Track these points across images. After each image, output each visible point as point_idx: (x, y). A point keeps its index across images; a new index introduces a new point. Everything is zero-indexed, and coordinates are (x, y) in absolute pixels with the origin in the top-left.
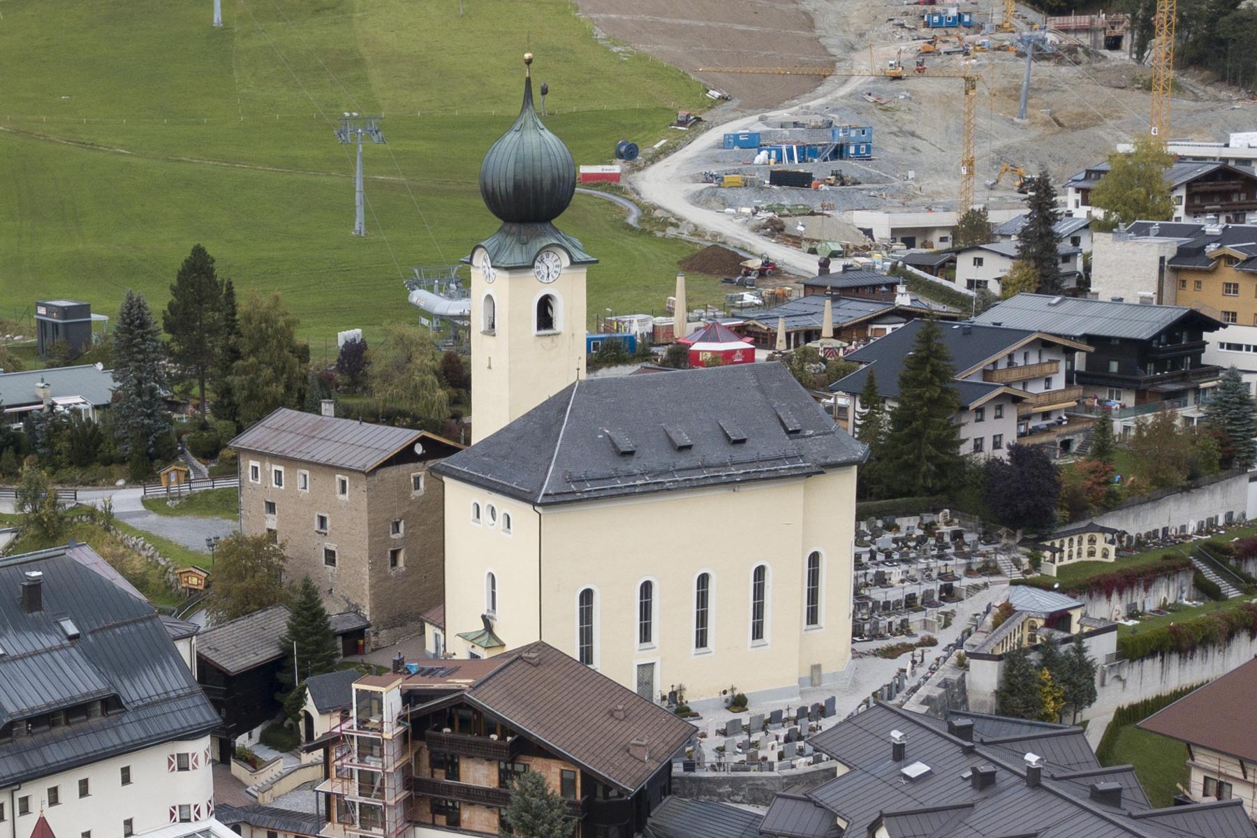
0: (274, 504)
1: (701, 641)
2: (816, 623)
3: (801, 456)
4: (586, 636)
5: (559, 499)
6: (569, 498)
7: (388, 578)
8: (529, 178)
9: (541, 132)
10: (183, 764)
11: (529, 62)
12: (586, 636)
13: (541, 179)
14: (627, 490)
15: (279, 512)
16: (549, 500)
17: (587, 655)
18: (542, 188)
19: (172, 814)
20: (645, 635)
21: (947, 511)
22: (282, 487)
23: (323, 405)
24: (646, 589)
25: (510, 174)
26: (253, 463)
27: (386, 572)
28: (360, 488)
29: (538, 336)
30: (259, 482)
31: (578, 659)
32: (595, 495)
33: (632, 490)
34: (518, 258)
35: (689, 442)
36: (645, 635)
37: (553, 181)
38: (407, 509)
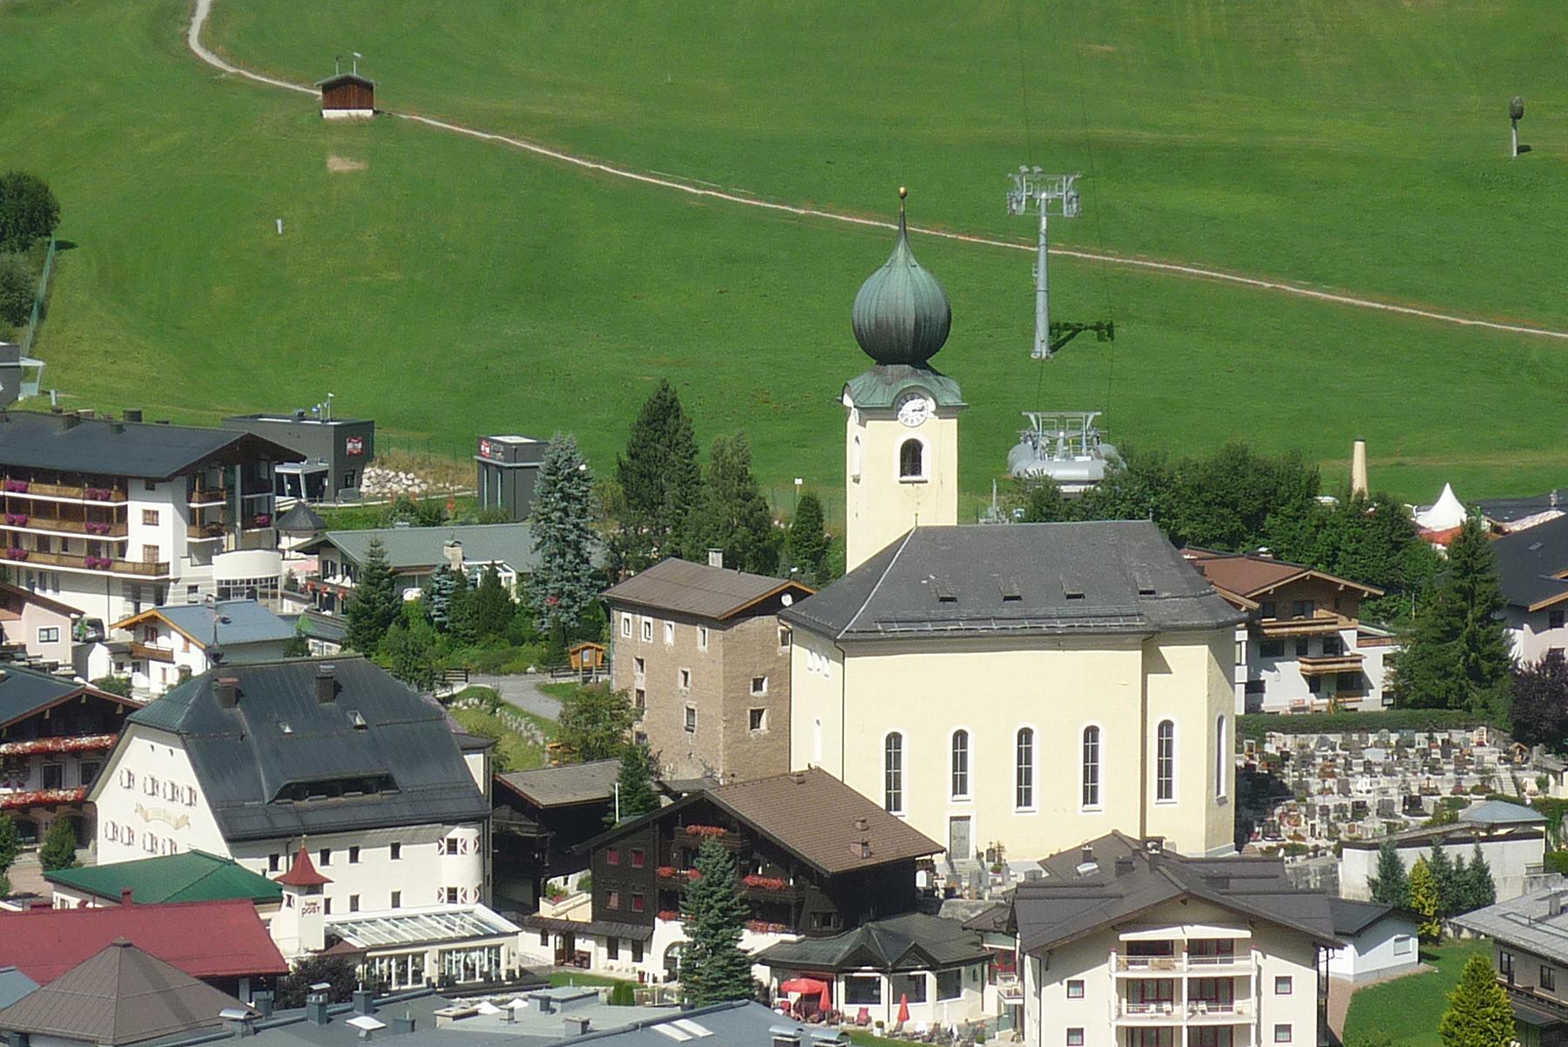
0: (1276, 1026)
1: (1024, 798)
2: (1170, 797)
3: (1139, 615)
4: (893, 782)
5: (860, 636)
6: (872, 636)
7: (746, 740)
8: (892, 318)
9: (912, 269)
10: (452, 847)
11: (903, 196)
12: (893, 782)
13: (904, 319)
14: (936, 634)
15: (648, 670)
16: (851, 636)
17: (894, 801)
18: (905, 328)
19: (440, 895)
20: (960, 785)
21: (1484, 728)
22: (651, 642)
23: (710, 554)
24: (960, 738)
25: (910, 304)
26: (625, 615)
27: (744, 732)
28: (717, 638)
29: (902, 482)
30: (630, 637)
31: (884, 808)
32: (900, 635)
33: (941, 633)
34: (881, 398)
35: (1017, 593)
36: (960, 785)
37: (917, 323)
38: (771, 666)
